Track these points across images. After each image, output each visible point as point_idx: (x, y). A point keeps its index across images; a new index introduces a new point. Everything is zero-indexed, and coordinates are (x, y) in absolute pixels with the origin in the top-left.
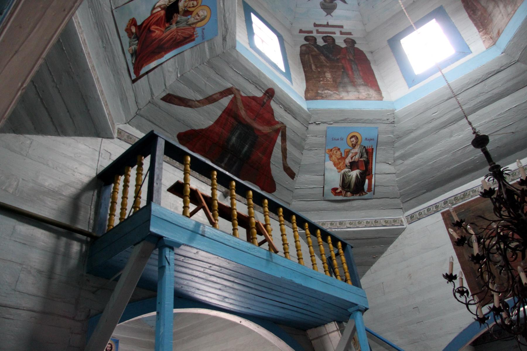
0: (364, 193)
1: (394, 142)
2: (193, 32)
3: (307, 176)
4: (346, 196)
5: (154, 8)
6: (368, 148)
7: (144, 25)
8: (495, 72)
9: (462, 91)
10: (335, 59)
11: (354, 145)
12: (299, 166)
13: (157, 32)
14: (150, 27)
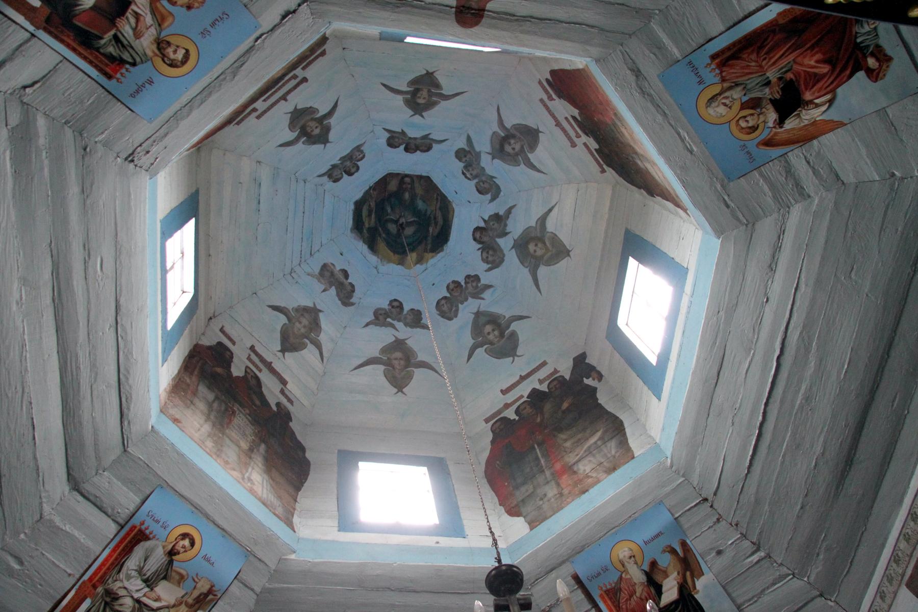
1: (81, 135)
2: (721, 72)
5: (831, 102)
6: (123, 71)
7: (848, 72)
8: (125, 411)
9: (120, 339)
11: (164, 46)
13: (811, 62)
14: (833, 71)
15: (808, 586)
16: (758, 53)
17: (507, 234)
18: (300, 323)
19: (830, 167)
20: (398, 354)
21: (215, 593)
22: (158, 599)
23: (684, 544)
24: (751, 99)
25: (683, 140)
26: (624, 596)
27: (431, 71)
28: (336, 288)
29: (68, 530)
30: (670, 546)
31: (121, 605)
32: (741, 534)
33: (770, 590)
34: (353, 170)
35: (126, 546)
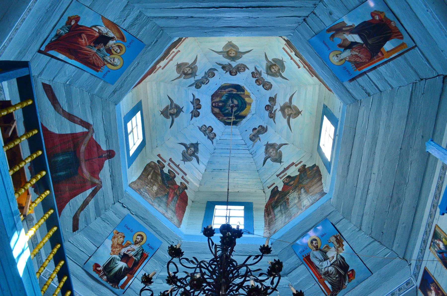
0: (116, 287)
3: (85, 238)
4: (101, 278)
5: (95, 26)
6: (145, 253)
7: (81, 28)
10: (167, 185)
12: (86, 226)
14: (83, 33)
16: (89, 58)
17: (229, 64)
18: (271, 152)
19: (123, 11)
20: (286, 111)
21: (337, 235)
22: (333, 257)
23: (329, 30)
24: (107, 53)
25: (135, 68)
26: (358, 60)
27: (161, 113)
28: (260, 134)
29: (299, 281)
30: (330, 38)
31: (331, 271)
34: (210, 129)
35: (310, 263)
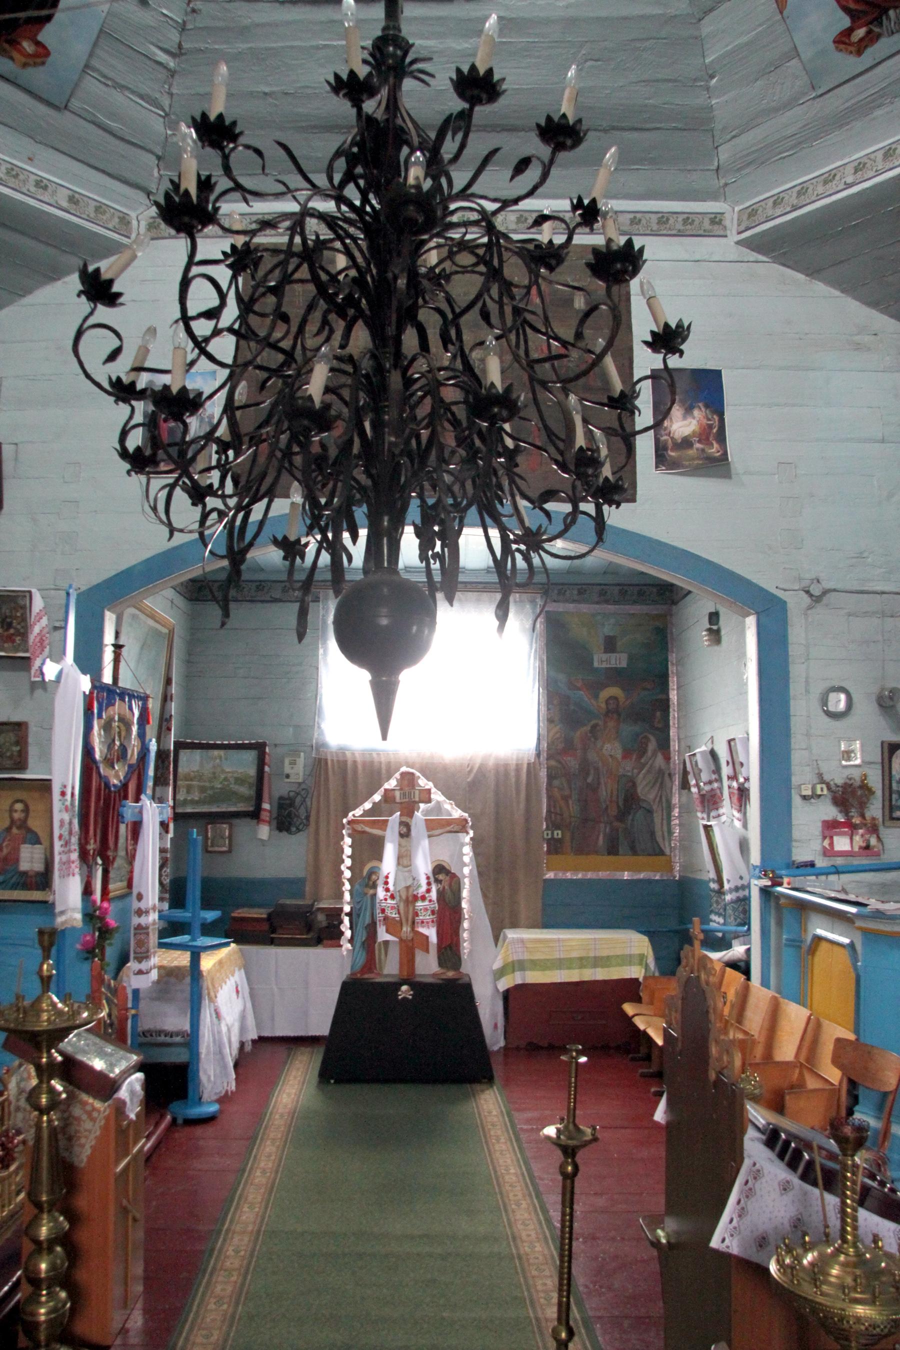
15: (163, 138)
32: (184, 22)
33: (131, 96)
